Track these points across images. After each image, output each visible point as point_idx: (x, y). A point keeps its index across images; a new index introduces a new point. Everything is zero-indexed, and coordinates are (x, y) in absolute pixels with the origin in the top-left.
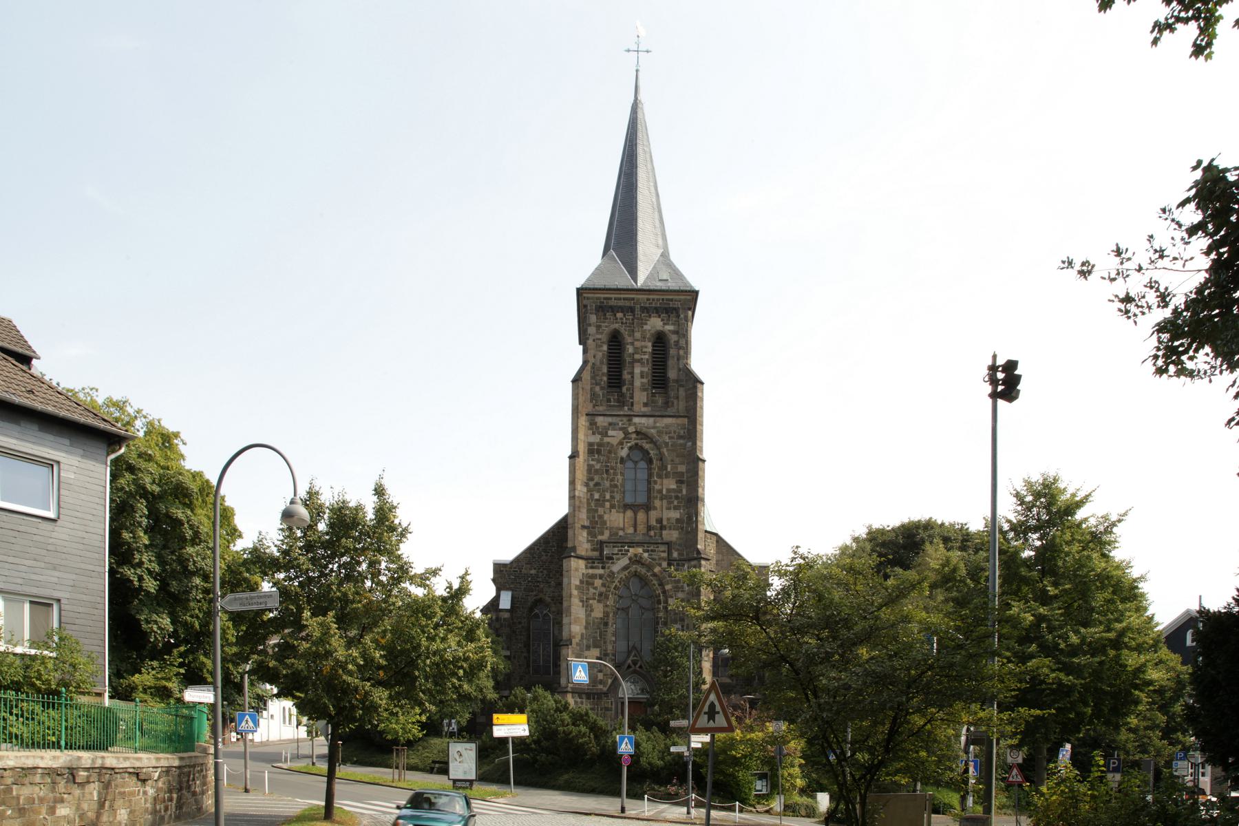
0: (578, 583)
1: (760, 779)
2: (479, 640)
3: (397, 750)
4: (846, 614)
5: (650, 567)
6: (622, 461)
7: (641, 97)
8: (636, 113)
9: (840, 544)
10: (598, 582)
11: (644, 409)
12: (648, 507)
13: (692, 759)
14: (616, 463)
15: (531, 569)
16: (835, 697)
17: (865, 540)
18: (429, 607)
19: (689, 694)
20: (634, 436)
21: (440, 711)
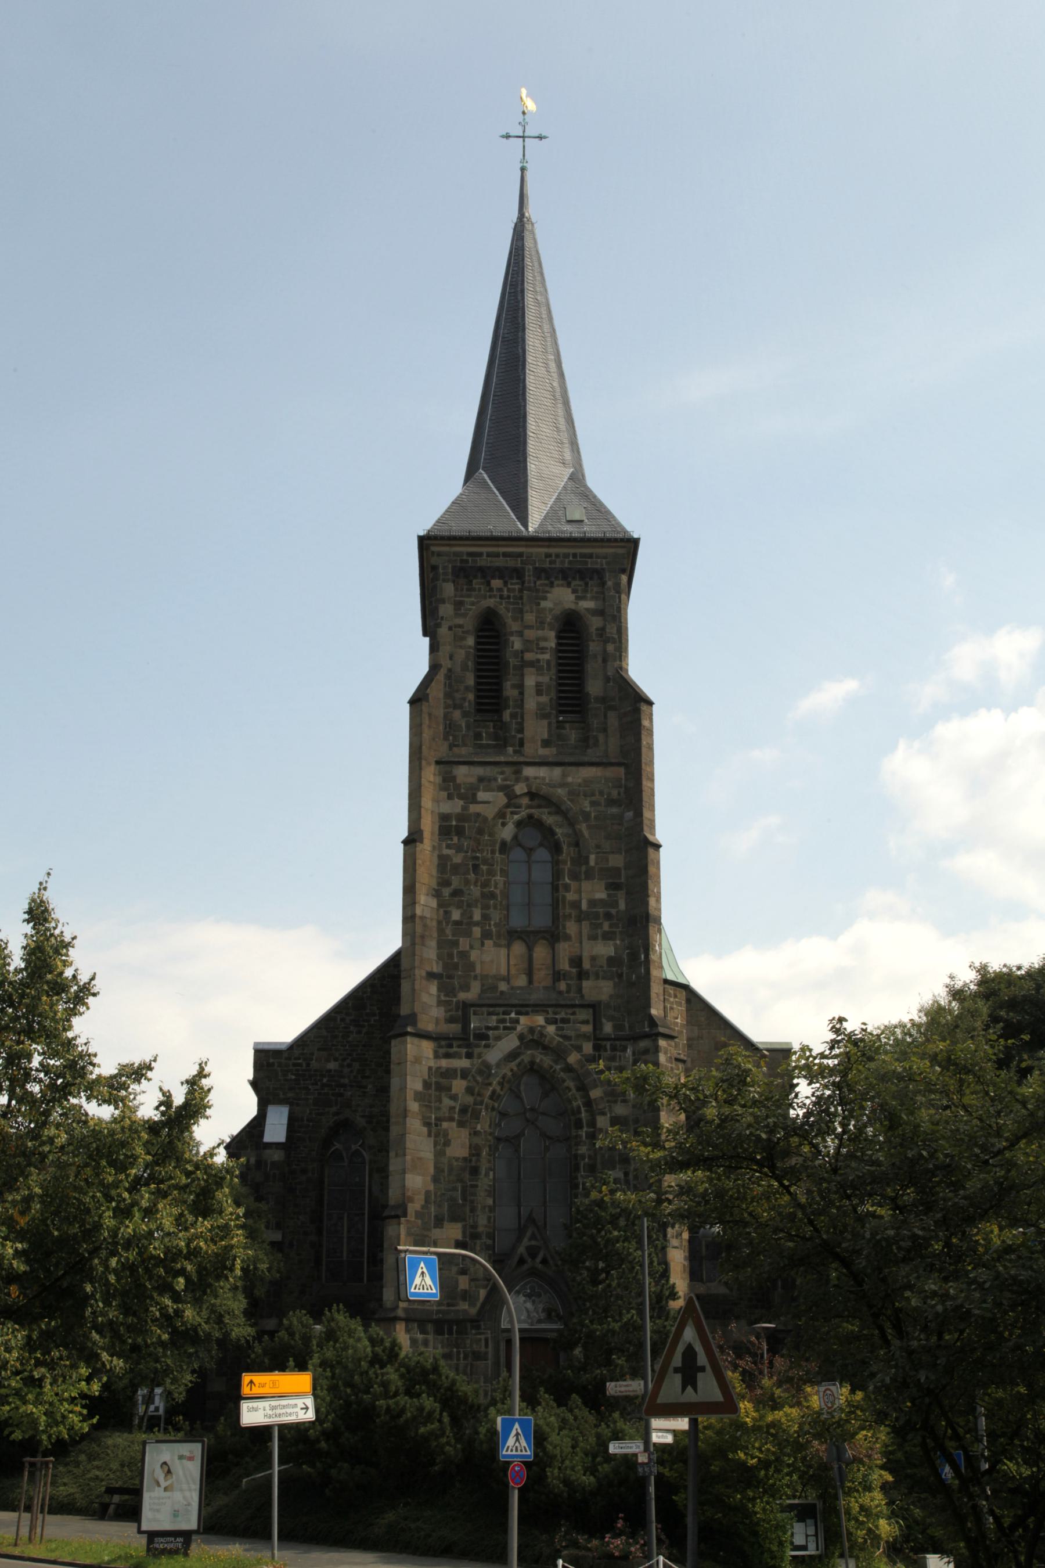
0: (419, 1086)
1: (801, 1519)
2: (221, 1212)
3: (32, 1465)
4: (946, 1156)
5: (559, 1054)
6: (504, 847)
7: (531, 212)
8: (523, 239)
9: (927, 1000)
10: (459, 1086)
11: (543, 752)
12: (553, 936)
13: (655, 1470)
14: (493, 852)
15: (328, 1061)
16: (940, 1337)
17: (975, 995)
18: (123, 1144)
19: (643, 1319)
20: (525, 801)
21: (132, 1370)
